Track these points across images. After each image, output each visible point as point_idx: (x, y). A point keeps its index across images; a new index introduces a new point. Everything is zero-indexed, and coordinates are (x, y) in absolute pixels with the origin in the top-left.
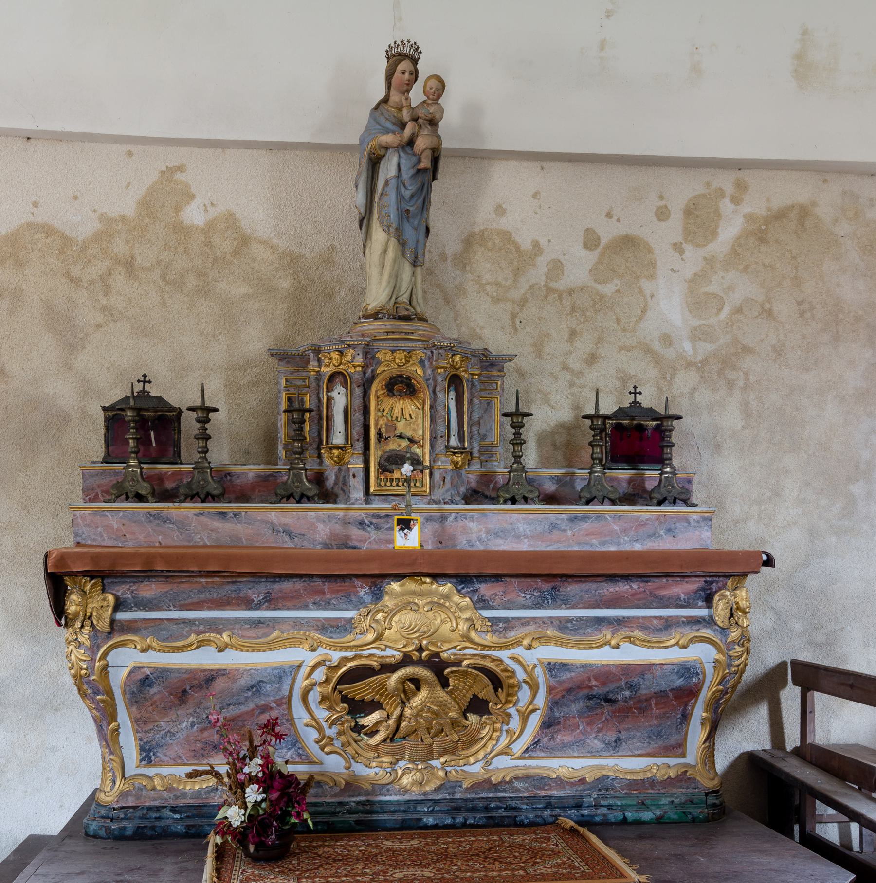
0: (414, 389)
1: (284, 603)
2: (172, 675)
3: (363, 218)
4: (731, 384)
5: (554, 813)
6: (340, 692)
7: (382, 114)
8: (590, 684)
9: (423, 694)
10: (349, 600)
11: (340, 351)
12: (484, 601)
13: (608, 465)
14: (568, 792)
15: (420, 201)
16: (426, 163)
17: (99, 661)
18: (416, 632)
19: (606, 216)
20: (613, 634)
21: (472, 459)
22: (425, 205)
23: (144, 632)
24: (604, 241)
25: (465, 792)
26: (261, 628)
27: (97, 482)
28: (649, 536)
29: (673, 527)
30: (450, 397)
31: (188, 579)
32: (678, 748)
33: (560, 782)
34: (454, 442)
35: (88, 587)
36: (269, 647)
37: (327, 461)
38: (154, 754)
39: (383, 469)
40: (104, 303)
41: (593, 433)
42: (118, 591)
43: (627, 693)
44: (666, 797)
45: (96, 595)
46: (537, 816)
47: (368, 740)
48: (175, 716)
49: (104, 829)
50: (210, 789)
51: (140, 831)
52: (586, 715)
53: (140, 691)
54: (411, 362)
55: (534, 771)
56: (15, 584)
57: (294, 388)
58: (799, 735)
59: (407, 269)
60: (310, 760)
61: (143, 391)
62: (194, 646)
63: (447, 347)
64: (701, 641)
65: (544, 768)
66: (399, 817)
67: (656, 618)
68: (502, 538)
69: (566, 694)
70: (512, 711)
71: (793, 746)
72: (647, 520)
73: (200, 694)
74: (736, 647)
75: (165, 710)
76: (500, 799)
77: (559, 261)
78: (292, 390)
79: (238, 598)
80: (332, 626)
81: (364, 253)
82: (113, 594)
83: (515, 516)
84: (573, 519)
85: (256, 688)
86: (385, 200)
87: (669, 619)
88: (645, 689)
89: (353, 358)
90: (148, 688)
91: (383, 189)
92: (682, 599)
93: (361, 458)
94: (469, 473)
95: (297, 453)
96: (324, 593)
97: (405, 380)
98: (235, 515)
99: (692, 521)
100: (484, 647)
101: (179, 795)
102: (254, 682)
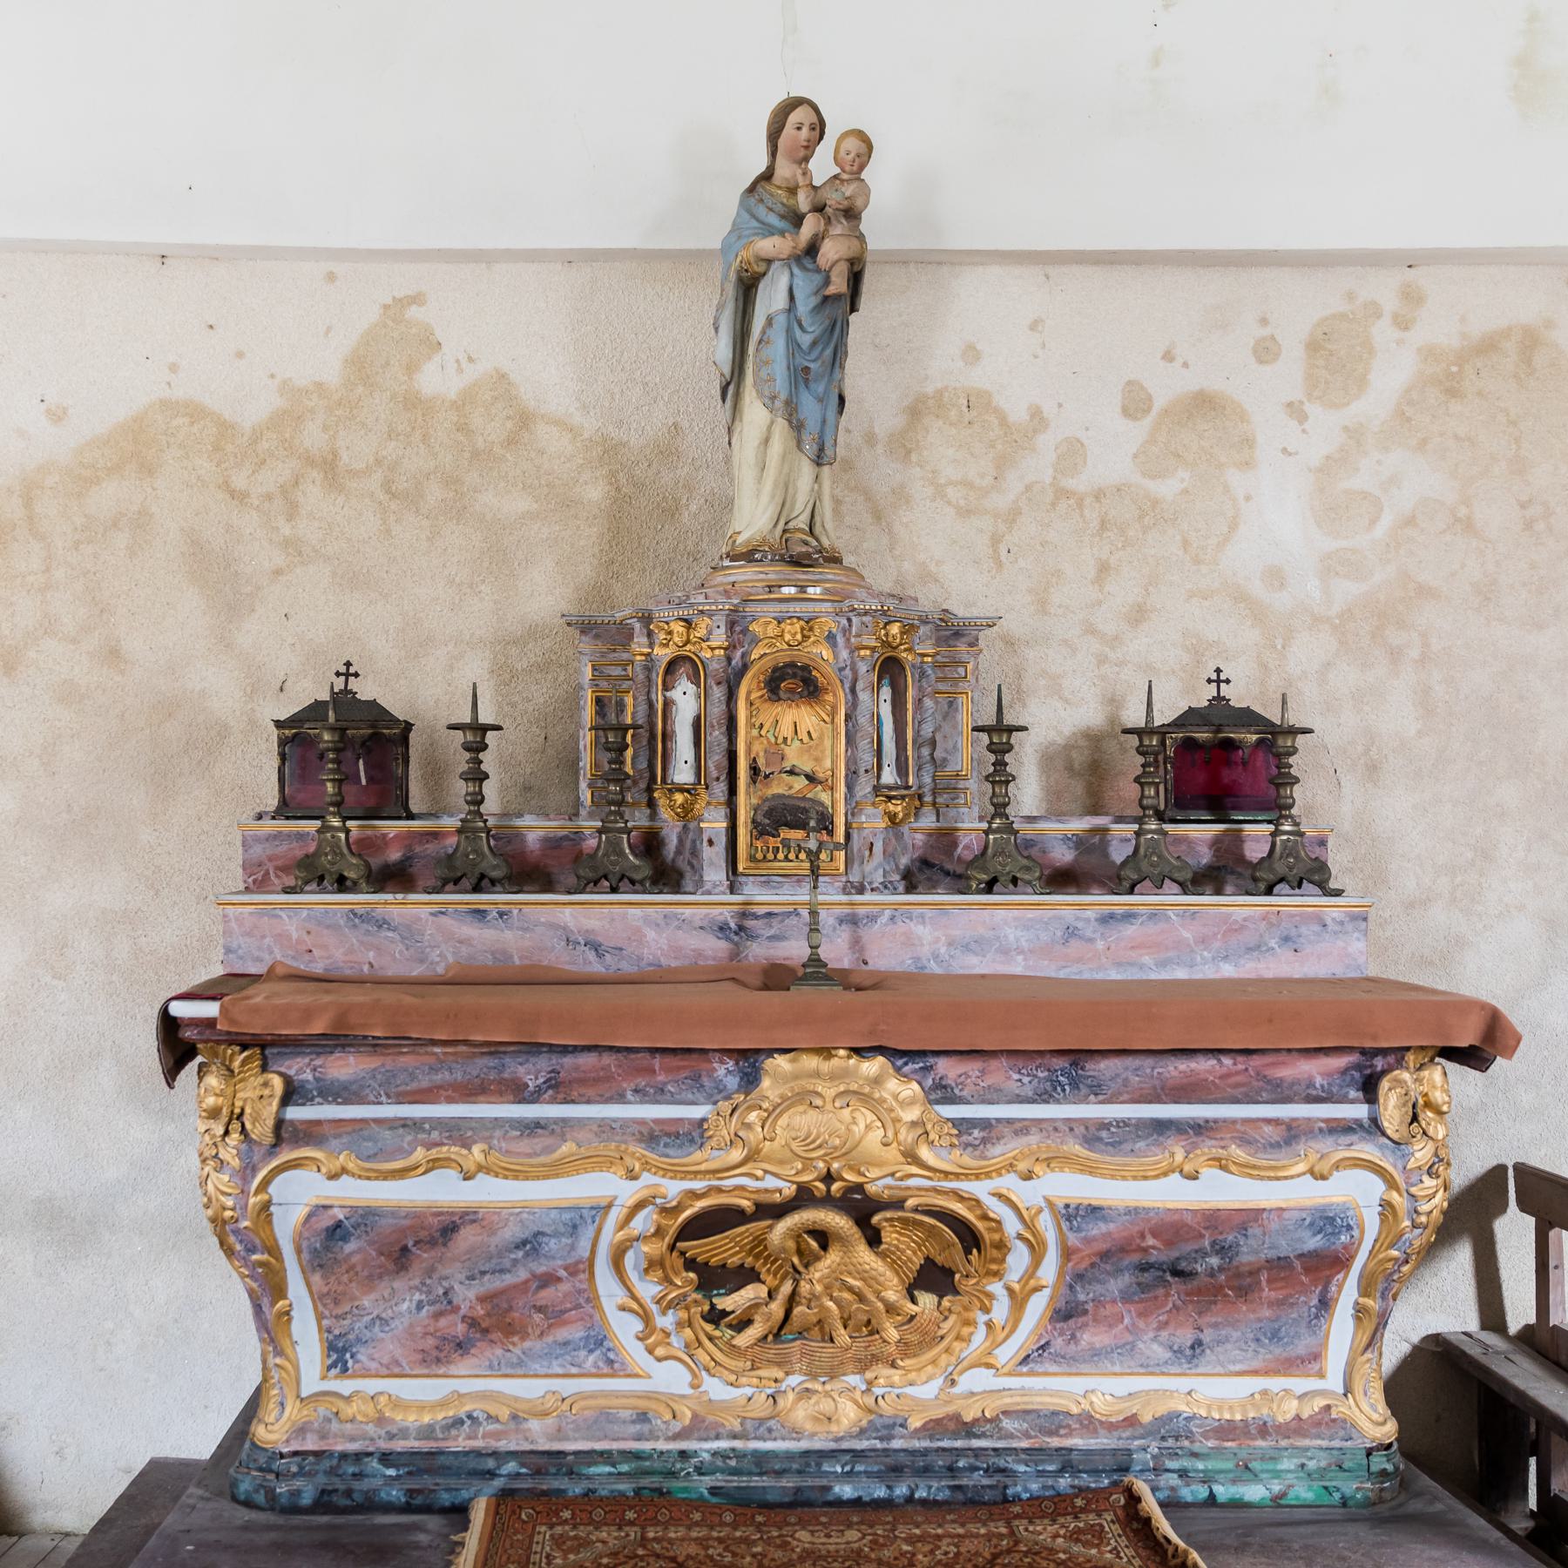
0: (816, 687)
1: (583, 1091)
2: (383, 1222)
3: (728, 384)
4: (1395, 655)
5: (1076, 1482)
6: (683, 1253)
7: (762, 201)
8: (1143, 1245)
9: (833, 1257)
10: (697, 1086)
11: (686, 620)
12: (945, 1087)
13: (1169, 814)
14: (1102, 1441)
15: (829, 352)
16: (839, 285)
17: (256, 1193)
18: (820, 1147)
19: (1163, 358)
20: (1188, 1153)
21: (922, 805)
22: (838, 357)
23: (334, 1143)
24: (1159, 403)
25: (912, 1438)
26: (540, 1136)
27: (269, 852)
28: (1250, 949)
29: (1293, 932)
30: (882, 697)
31: (411, 1049)
32: (1311, 1361)
33: (1088, 1422)
34: (889, 776)
35: (236, 1064)
36: (554, 1171)
37: (665, 813)
38: (352, 1357)
39: (761, 830)
40: (287, 533)
41: (1141, 760)
42: (289, 1067)
43: (1214, 1261)
44: (1290, 1457)
45: (250, 1076)
46: (1044, 1487)
47: (733, 1337)
48: (389, 1290)
49: (262, 1492)
50: (450, 1421)
51: (326, 1498)
52: (1136, 1298)
53: (327, 1249)
54: (812, 639)
55: (1039, 1399)
56: (134, 1017)
57: (607, 680)
58: (1534, 1303)
59: (806, 469)
60: (629, 1372)
61: (346, 691)
62: (421, 1170)
63: (876, 611)
64: (1356, 1166)
65: (1057, 1393)
66: (788, 1483)
67: (1268, 1121)
68: (976, 954)
69: (1098, 1261)
70: (996, 1288)
71: (1523, 1323)
72: (1245, 920)
73: (433, 1253)
74: (1425, 1178)
75: (370, 1281)
76: (977, 1453)
77: (1078, 441)
78: (604, 684)
79: (501, 1082)
80: (668, 1135)
81: (730, 443)
82: (280, 1074)
83: (1001, 914)
84: (1107, 919)
85: (530, 1245)
86: (767, 352)
87: (1294, 1125)
88: (1248, 1253)
89: (710, 633)
90: (340, 1243)
91: (764, 332)
92: (1318, 1085)
93: (722, 812)
94: (915, 830)
95: (611, 804)
96: (654, 1071)
97: (800, 673)
98: (501, 914)
99: (1329, 921)
100: (946, 1175)
101: (395, 1431)
102: (527, 1234)
